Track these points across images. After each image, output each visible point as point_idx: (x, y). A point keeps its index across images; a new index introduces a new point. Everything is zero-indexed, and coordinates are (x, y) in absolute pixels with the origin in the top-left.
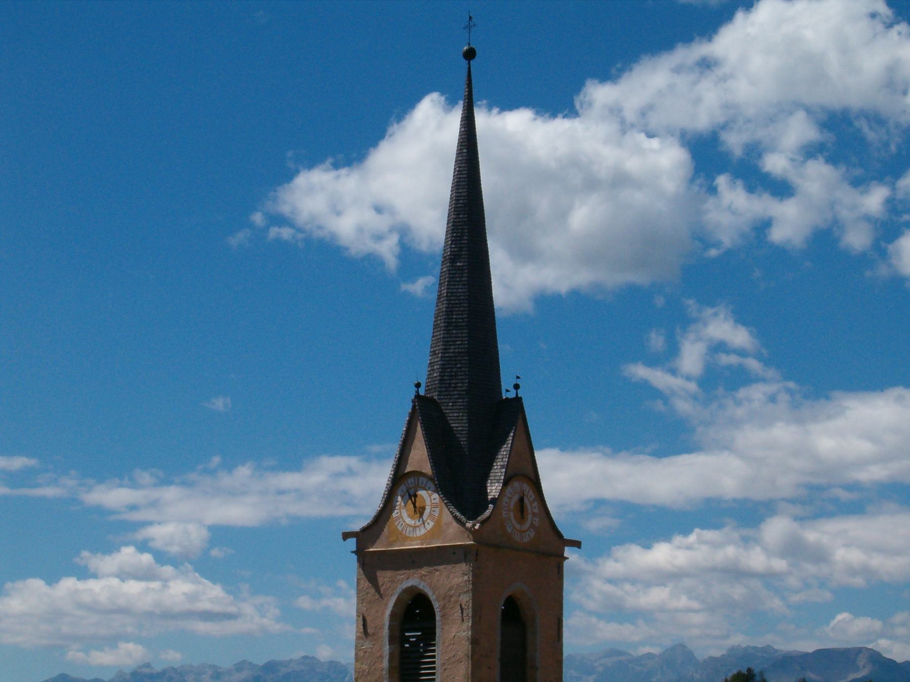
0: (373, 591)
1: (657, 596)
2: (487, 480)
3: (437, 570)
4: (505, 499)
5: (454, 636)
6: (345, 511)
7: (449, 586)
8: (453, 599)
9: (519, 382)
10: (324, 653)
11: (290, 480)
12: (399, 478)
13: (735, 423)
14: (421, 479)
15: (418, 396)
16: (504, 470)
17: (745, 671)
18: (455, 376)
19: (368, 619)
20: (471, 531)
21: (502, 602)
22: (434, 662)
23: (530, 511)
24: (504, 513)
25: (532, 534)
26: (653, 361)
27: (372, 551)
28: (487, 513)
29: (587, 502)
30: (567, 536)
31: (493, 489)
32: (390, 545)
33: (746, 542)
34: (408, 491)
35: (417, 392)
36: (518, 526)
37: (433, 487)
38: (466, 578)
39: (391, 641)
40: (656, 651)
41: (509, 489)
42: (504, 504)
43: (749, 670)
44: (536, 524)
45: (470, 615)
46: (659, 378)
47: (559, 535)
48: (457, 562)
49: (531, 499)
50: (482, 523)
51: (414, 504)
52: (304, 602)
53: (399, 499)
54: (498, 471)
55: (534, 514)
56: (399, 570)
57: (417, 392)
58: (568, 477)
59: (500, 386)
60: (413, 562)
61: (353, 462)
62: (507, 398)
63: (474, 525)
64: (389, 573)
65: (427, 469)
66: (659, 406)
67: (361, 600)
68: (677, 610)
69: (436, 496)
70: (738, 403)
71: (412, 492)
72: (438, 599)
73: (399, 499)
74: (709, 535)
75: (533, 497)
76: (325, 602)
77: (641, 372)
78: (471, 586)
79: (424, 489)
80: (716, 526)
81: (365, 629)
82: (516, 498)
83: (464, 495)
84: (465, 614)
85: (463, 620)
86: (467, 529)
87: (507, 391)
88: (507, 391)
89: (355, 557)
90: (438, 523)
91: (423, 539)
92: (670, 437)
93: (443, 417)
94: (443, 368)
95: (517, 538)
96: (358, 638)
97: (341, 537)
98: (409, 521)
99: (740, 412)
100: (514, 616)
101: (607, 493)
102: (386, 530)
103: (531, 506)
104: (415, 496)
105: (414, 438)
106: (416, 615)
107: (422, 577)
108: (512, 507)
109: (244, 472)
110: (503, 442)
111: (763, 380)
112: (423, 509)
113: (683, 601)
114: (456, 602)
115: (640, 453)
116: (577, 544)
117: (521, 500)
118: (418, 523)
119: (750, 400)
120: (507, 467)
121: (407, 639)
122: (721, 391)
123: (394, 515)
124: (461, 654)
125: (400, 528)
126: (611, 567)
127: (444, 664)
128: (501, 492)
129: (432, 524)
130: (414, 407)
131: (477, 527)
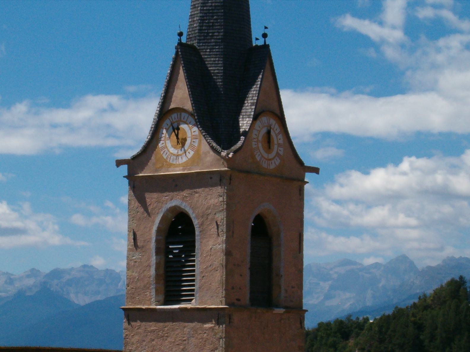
0: (141, 210)
1: (378, 215)
2: (239, 116)
3: (197, 193)
4: (255, 132)
5: (211, 250)
6: (111, 142)
7: (207, 207)
8: (210, 217)
9: (266, 31)
10: (99, 263)
11: (62, 116)
12: (164, 113)
13: (435, 67)
14: (183, 114)
15: (180, 44)
16: (253, 107)
17: (457, 278)
18: (213, 26)
19: (138, 234)
20: (227, 160)
21: (252, 219)
22: (194, 271)
23: (276, 142)
24: (254, 143)
25: (278, 161)
26: (361, 15)
27: (141, 176)
28: (240, 144)
29: (315, 135)
30: (307, 164)
31: (245, 124)
32: (156, 171)
33: (454, 169)
34: (172, 124)
35: (180, 40)
36: (265, 155)
37: (194, 122)
38: (221, 199)
39: (158, 252)
40: (379, 260)
41: (258, 123)
42: (254, 136)
43: (461, 278)
44: (281, 153)
45: (225, 230)
46: (369, 28)
47: (301, 163)
48: (214, 185)
49: (277, 132)
50: (235, 152)
51: (177, 136)
52: (78, 219)
53: (164, 131)
54: (249, 108)
55: (279, 145)
56: (164, 192)
57: (180, 40)
58: (305, 113)
59: (251, 35)
60: (176, 185)
61: (114, 100)
62: (256, 46)
63: (228, 154)
64: (155, 195)
65: (188, 106)
66: (372, 53)
67: (132, 218)
68: (397, 227)
69: (195, 129)
70: (439, 50)
71: (175, 125)
72: (197, 217)
73: (164, 131)
74: (422, 162)
75: (279, 130)
76: (95, 220)
77: (349, 22)
78: (225, 206)
79: (185, 123)
80: (239, 148)
81: (135, 242)
82: (264, 131)
83: (219, 126)
84: (220, 230)
85: (218, 235)
86: (222, 157)
87: (257, 39)
88: (257, 39)
89: (126, 181)
90: (197, 152)
91: (185, 165)
92: (386, 81)
93: (202, 61)
94: (202, 20)
95: (265, 165)
96: (129, 250)
97: (115, 164)
98: (172, 150)
99: (440, 58)
100: (261, 230)
101: (332, 127)
102: (153, 158)
103: (277, 138)
104: (178, 129)
105: (177, 80)
106: (179, 231)
107: (184, 199)
108: (260, 138)
109: (21, 108)
110: (253, 82)
111: (461, 32)
112: (185, 140)
113: (402, 219)
114: (213, 219)
115: (362, 93)
116: (316, 170)
117: (269, 133)
118: (180, 152)
119: (449, 48)
120: (256, 104)
121: (170, 251)
122: (423, 38)
123: (160, 145)
124: (216, 264)
125: (165, 157)
126: (337, 191)
127: (202, 272)
128: (252, 126)
129: (192, 153)
130: (177, 54)
131: (230, 156)
